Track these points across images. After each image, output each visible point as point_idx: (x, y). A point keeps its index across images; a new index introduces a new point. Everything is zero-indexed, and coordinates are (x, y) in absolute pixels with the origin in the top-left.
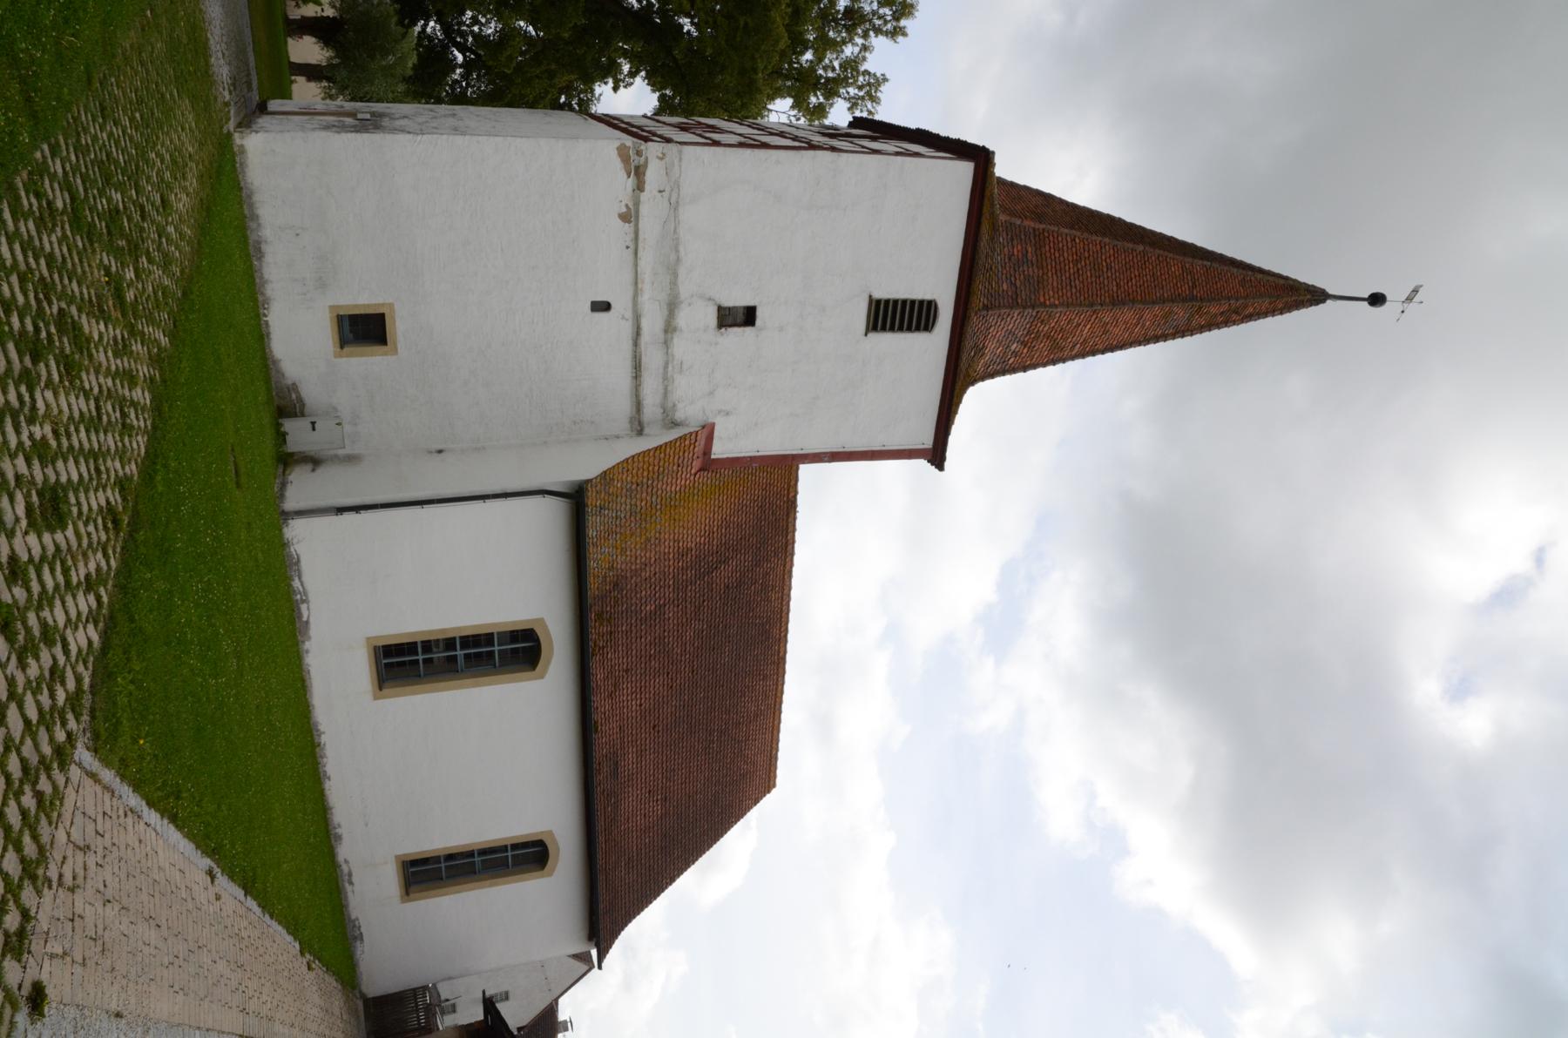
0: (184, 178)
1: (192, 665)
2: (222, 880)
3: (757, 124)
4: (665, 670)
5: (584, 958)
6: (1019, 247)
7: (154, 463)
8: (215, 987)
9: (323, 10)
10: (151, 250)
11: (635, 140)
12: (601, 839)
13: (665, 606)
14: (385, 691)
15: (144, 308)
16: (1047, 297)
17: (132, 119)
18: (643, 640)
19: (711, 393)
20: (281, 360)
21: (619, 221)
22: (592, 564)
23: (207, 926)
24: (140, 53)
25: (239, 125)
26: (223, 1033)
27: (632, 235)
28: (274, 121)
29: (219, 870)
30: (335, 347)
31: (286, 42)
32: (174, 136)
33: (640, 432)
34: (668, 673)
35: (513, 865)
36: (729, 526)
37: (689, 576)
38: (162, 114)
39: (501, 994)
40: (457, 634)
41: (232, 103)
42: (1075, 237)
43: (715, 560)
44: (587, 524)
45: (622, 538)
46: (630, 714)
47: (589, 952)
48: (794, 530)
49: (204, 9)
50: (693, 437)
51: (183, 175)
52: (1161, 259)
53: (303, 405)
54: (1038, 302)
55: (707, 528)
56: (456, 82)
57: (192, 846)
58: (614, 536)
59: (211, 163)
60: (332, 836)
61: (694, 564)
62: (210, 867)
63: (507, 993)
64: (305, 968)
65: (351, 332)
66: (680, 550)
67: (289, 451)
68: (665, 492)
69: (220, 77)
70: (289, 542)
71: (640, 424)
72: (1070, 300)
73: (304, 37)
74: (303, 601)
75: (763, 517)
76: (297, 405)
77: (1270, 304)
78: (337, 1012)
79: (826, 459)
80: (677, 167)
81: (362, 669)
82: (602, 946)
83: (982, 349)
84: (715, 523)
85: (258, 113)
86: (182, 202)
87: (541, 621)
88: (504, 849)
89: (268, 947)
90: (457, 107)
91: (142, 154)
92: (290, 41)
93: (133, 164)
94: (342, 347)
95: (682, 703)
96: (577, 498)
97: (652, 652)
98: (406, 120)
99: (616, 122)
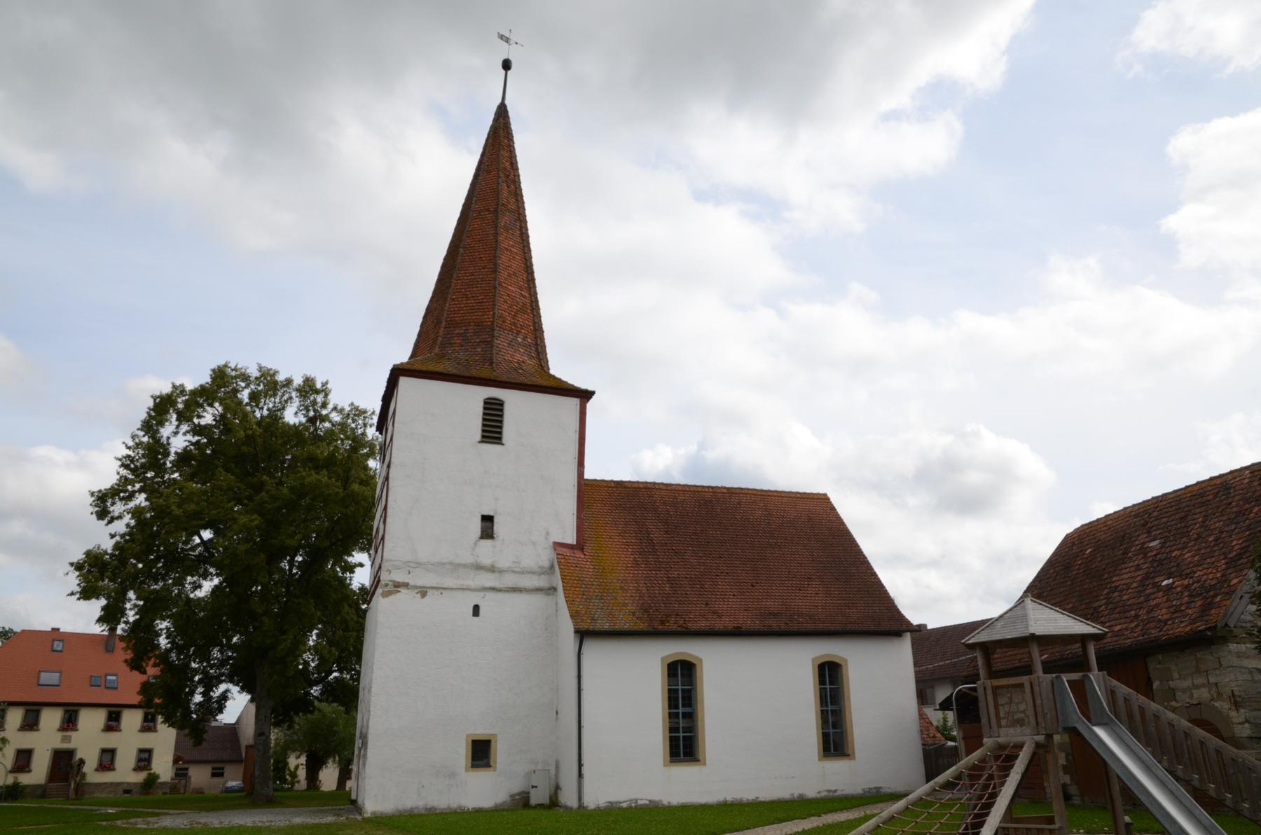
6: (456, 338)
9: (302, 764)
14: (701, 757)
16: (488, 320)
19: (534, 544)
22: (626, 627)
34: (717, 575)
42: (451, 298)
50: (559, 556)
52: (469, 235)
53: (523, 792)
54: (491, 326)
65: (482, 760)
72: (491, 303)
74: (636, 802)
77: (504, 149)
80: (395, 563)
81: (685, 772)
83: (518, 363)
84: (620, 540)
87: (663, 659)
94: (490, 766)
96: (583, 634)
97: (699, 586)
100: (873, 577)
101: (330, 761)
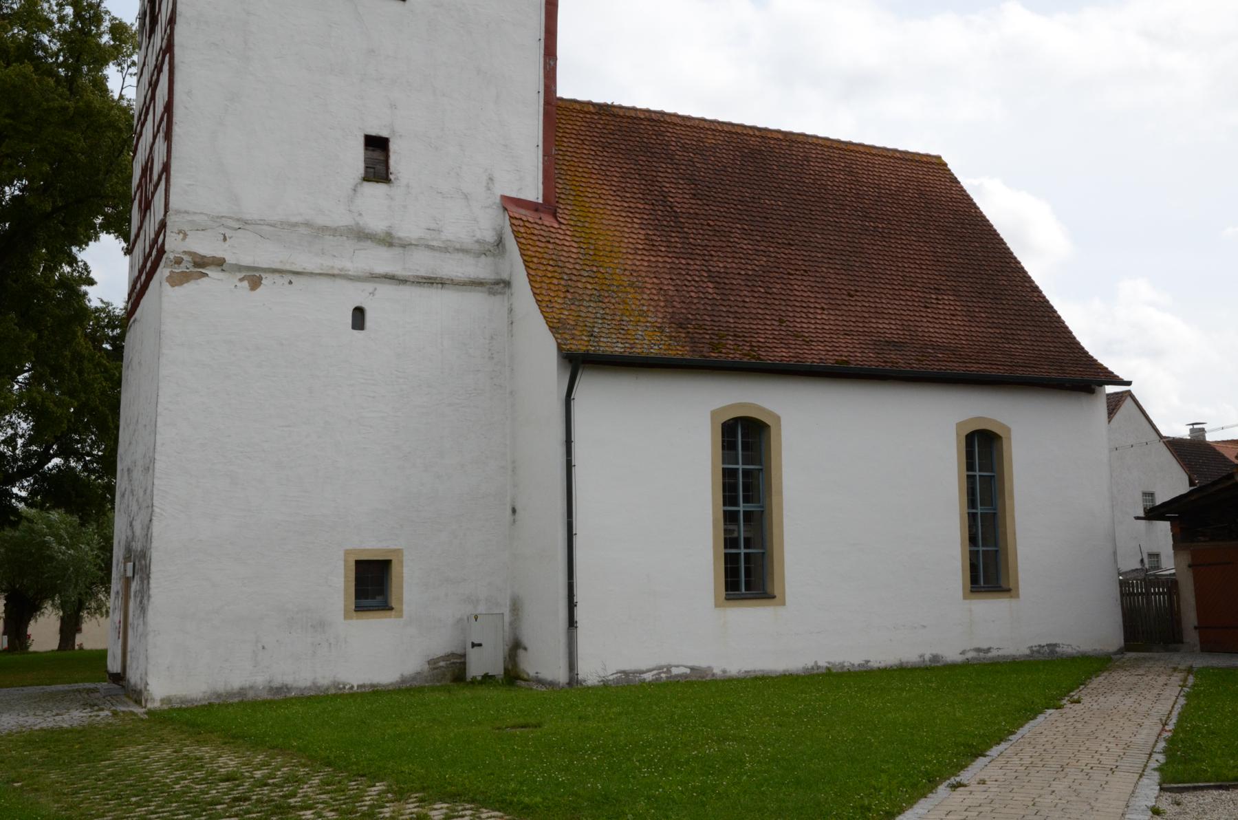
0: (201, 758)
1: (728, 783)
2: (964, 776)
3: (140, 115)
4: (785, 277)
5: (1115, 403)
7: (511, 803)
8: (1080, 795)
10: (281, 794)
11: (162, 264)
12: (974, 368)
13: (710, 271)
14: (776, 593)
15: (344, 804)
17: (138, 805)
18: (747, 300)
19: (466, 197)
20: (402, 675)
21: (259, 290)
22: (654, 351)
23: (1011, 795)
24: (64, 794)
25: (138, 702)
26: (1133, 792)
27: (277, 276)
28: (134, 665)
29: (952, 779)
30: (390, 617)
31: (35, 653)
32: (155, 766)
33: (507, 284)
34: (789, 274)
35: (992, 471)
36: (624, 188)
37: (677, 239)
38: (130, 776)
39: (1145, 501)
40: (721, 509)
41: (114, 708)
43: (661, 208)
44: (608, 353)
45: (628, 314)
46: (832, 322)
47: (1108, 395)
48: (634, 109)
49: (6, 731)
51: (198, 759)
53: (453, 655)
55: (624, 214)
56: (85, 467)
57: (923, 801)
58: (624, 323)
59: (183, 732)
60: (933, 665)
61: (664, 233)
62: (948, 786)
63: (1145, 494)
64: (1077, 706)
66: (647, 247)
67: (502, 672)
68: (578, 261)
69: (84, 719)
70: (602, 681)
71: (497, 283)
73: (28, 633)
74: (669, 671)
75: (616, 146)
76: (452, 661)
78: (1134, 679)
79: (552, 63)
80: (196, 218)
82: (1103, 378)
84: (618, 204)
85: (124, 683)
86: (228, 762)
88: (971, 479)
89: (1046, 739)
90: (119, 467)
91: (177, 797)
92: (32, 649)
93: (188, 806)
95: (825, 261)
97: (762, 290)
98: (134, 523)
99: (138, 286)
100: (1035, 294)
101: (48, 605)
